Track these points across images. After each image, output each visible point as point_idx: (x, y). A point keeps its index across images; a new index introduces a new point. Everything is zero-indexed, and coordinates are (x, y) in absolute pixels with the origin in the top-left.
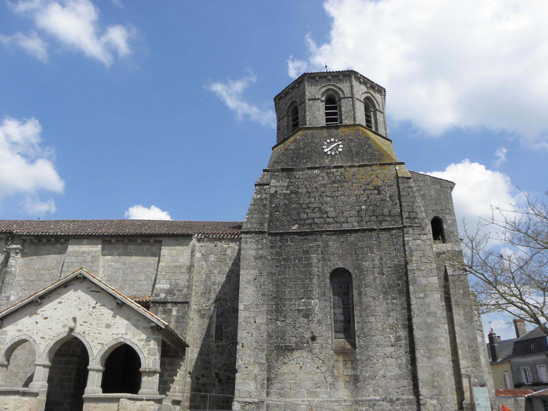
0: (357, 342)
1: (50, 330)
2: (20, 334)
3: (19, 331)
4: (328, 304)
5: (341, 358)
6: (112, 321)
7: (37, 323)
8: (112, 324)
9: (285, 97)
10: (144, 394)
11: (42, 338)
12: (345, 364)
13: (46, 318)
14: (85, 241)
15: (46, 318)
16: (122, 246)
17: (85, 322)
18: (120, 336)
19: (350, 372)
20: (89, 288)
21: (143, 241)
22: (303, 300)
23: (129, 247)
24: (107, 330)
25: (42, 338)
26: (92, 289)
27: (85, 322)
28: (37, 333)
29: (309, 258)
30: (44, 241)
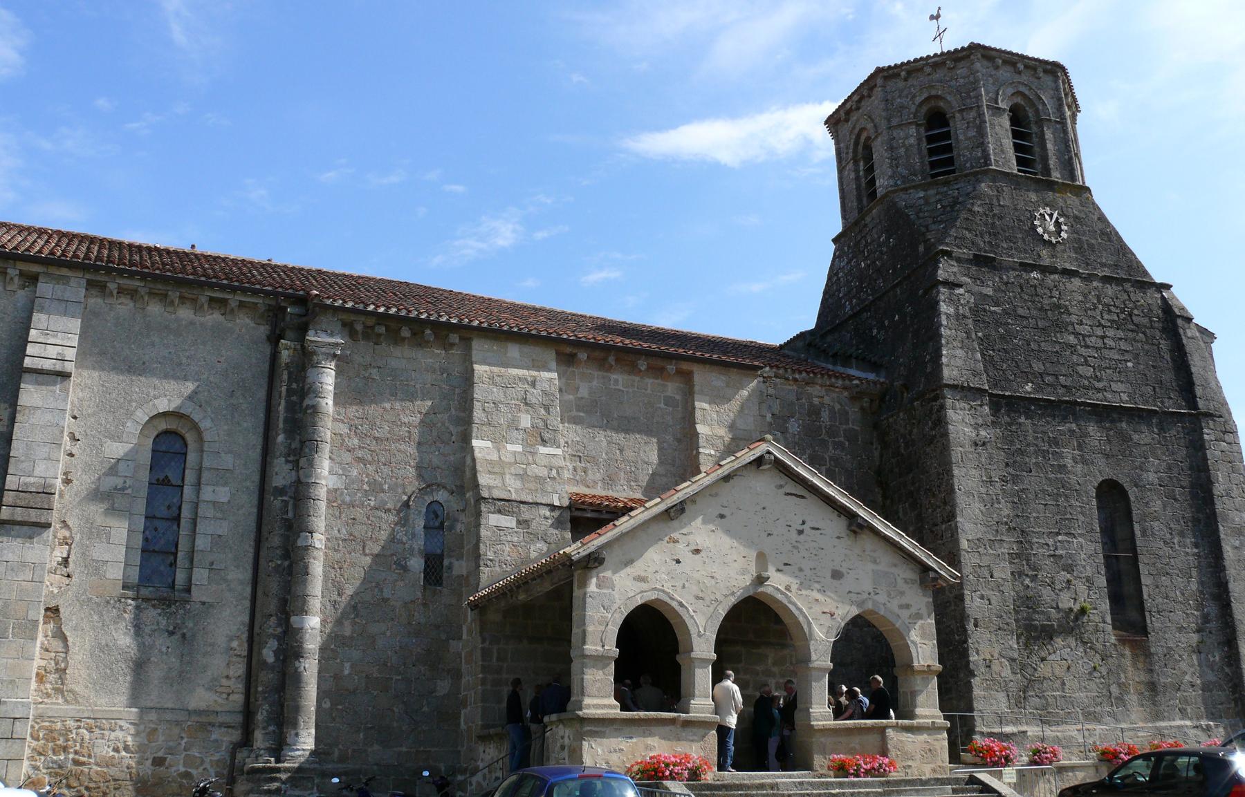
0: (1148, 621)
1: (713, 581)
2: (645, 586)
3: (641, 579)
4: (490, 555)
5: (1128, 652)
6: (844, 564)
7: (678, 562)
8: (843, 570)
9: (906, 80)
10: (926, 717)
11: (698, 598)
12: (1134, 665)
13: (697, 551)
14: (514, 350)
15: (697, 551)
16: (596, 373)
17: (786, 564)
18: (865, 596)
19: (1143, 677)
20: (781, 486)
21: (650, 368)
22: (1060, 538)
23: (614, 376)
24: (836, 583)
25: (698, 598)
26: (788, 489)
27: (786, 564)
28: (684, 587)
29: (1059, 455)
30: (406, 333)
